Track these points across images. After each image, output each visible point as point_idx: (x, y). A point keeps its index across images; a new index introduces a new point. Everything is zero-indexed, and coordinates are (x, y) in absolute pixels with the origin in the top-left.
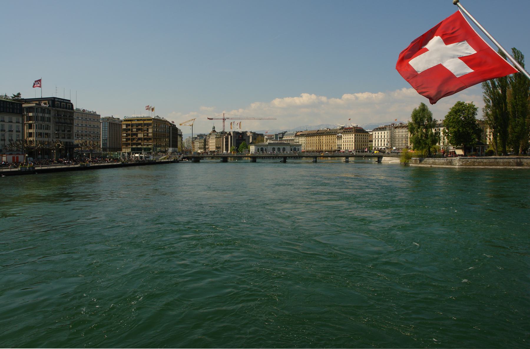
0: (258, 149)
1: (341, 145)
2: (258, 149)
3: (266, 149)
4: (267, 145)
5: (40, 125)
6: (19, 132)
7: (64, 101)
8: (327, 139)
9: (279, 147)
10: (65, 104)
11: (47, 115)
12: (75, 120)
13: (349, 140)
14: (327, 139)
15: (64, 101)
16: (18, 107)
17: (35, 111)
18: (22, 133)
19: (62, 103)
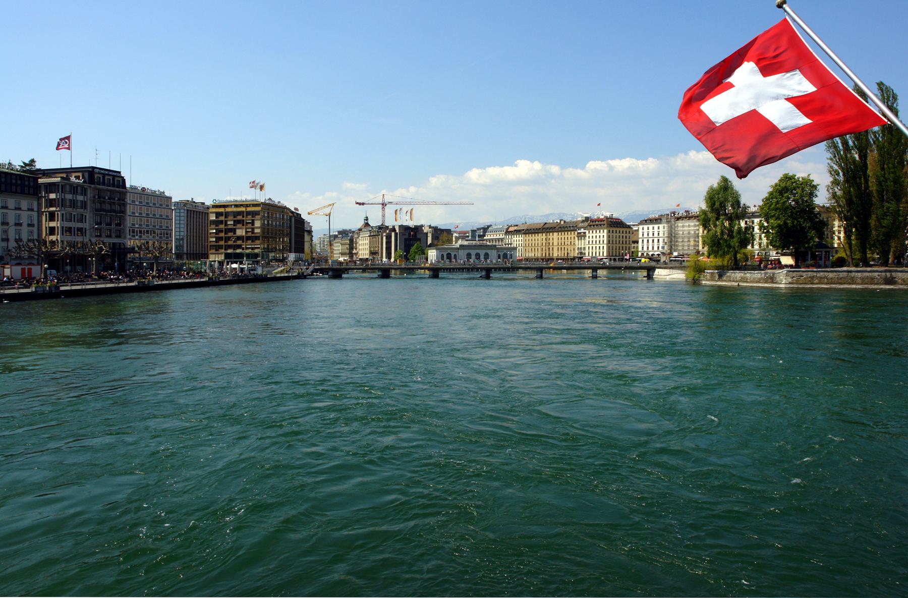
0: (443, 255)
1: (584, 248)
2: (443, 255)
3: (455, 256)
4: (458, 249)
5: (68, 214)
6: (33, 225)
7: (110, 173)
8: (560, 239)
9: (478, 251)
10: (111, 178)
11: (80, 198)
12: (128, 206)
13: (598, 239)
14: (560, 239)
15: (110, 173)
16: (32, 184)
17: (60, 190)
18: (38, 227)
19: (107, 177)
